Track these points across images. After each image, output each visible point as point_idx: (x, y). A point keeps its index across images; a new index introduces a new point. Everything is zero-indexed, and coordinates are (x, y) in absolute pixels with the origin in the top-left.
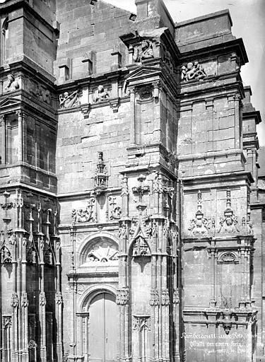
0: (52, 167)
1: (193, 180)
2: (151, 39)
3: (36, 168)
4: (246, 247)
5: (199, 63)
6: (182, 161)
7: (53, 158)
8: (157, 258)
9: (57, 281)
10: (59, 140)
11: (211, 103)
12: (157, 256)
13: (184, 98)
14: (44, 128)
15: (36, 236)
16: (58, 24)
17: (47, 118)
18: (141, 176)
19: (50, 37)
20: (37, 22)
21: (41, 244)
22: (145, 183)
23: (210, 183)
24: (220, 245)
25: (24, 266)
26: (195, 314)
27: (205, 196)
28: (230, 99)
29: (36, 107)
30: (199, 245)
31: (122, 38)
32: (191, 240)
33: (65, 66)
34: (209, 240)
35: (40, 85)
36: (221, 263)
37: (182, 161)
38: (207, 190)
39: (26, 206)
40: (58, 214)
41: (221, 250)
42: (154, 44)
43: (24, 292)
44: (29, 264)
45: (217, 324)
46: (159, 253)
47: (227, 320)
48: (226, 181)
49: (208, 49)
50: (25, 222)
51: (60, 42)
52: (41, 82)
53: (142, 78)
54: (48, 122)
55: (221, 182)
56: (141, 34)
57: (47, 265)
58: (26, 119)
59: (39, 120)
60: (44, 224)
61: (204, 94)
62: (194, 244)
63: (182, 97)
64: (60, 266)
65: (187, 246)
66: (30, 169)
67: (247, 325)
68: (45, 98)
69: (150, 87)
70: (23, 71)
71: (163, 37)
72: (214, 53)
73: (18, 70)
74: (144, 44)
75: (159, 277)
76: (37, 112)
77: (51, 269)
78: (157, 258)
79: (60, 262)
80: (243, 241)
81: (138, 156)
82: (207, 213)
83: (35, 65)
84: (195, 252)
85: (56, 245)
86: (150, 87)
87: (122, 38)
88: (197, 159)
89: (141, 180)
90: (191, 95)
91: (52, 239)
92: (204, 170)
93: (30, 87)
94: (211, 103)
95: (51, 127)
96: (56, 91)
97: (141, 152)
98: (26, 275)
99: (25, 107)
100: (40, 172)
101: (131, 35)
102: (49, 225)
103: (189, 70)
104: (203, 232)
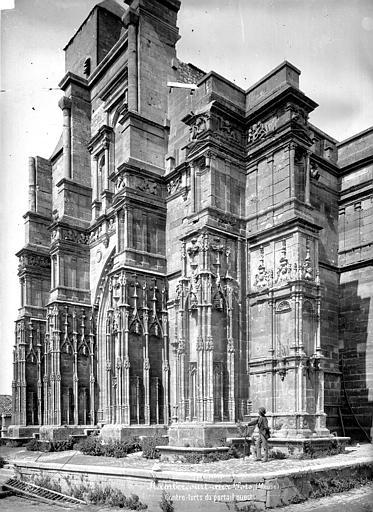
0: (162, 250)
1: (255, 237)
2: (203, 115)
3: (143, 252)
4: (296, 293)
5: (263, 122)
6: (248, 220)
7: (163, 242)
8: (202, 310)
9: (164, 351)
10: (168, 224)
11: (271, 159)
12: (202, 307)
13: (251, 159)
14: (153, 216)
15: (140, 310)
16: (168, 121)
17: (156, 208)
18: (194, 239)
19: (161, 135)
20: (145, 126)
21: (145, 317)
22: (197, 244)
23: (270, 236)
24: (276, 295)
25: (127, 334)
26: (257, 364)
27: (267, 250)
28: (287, 149)
29: (143, 200)
30: (261, 298)
31: (184, 120)
32: (254, 295)
33: (171, 158)
34: (266, 292)
35: (146, 179)
36: (279, 312)
37: (248, 220)
38: (267, 244)
39: (130, 285)
40: (167, 291)
41: (278, 299)
42: (205, 119)
43: (127, 356)
44: (132, 333)
45: (274, 372)
46: (204, 304)
47: (280, 366)
48: (280, 231)
49: (266, 106)
50: (129, 299)
51: (170, 137)
52: (147, 177)
53: (198, 152)
54: (157, 211)
55: (278, 233)
56: (196, 114)
57: (152, 336)
58: (132, 212)
59: (147, 212)
60: (150, 299)
61: (265, 151)
62: (257, 298)
63: (249, 159)
64: (167, 337)
65: (253, 301)
66: (135, 253)
67: (296, 368)
68: (152, 190)
69: (202, 158)
70: (128, 171)
71: (212, 109)
72: (273, 109)
73: (124, 171)
74: (198, 121)
75: (204, 326)
76: (143, 204)
77: (157, 340)
78: (202, 310)
79: (168, 333)
80: (293, 288)
81: (195, 222)
82: (269, 267)
83: (142, 164)
84: (259, 306)
85: (164, 319)
86: (202, 158)
87: (184, 120)
88: (261, 216)
89: (194, 242)
90: (256, 155)
91: (159, 313)
92: (265, 225)
93: (136, 182)
94: (271, 159)
95: (159, 215)
96: (163, 182)
97: (196, 218)
98: (335, 471)
99: (131, 201)
100: (147, 255)
101: (189, 116)
102: (156, 302)
103: (254, 131)
104: (265, 284)
